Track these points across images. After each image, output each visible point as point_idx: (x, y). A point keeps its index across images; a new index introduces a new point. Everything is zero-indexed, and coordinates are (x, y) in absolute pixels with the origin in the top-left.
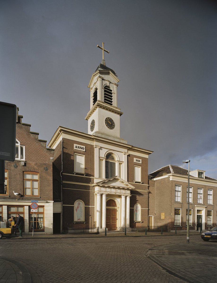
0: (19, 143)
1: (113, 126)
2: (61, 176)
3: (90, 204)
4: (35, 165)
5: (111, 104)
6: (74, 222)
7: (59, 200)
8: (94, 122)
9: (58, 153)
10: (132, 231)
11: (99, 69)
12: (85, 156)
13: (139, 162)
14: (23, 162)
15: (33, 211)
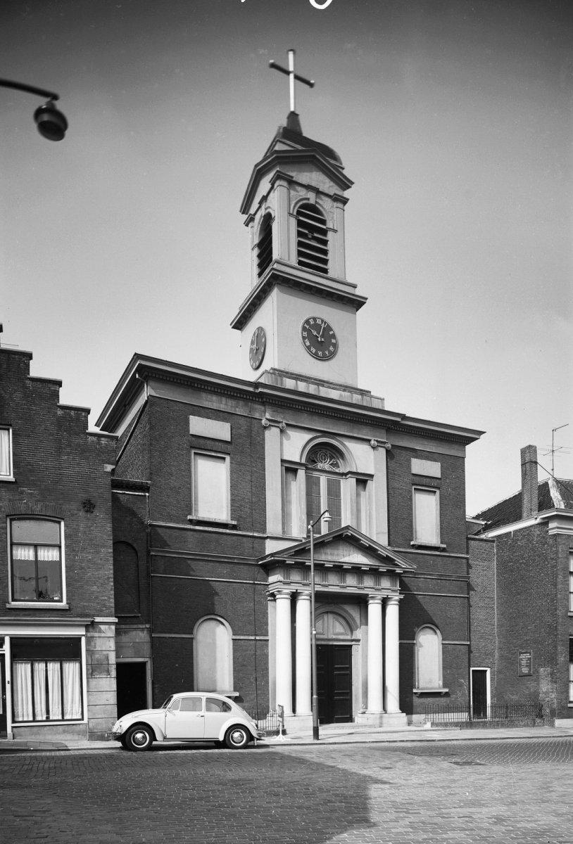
5: (325, 271)
7: (140, 615)
8: (265, 336)
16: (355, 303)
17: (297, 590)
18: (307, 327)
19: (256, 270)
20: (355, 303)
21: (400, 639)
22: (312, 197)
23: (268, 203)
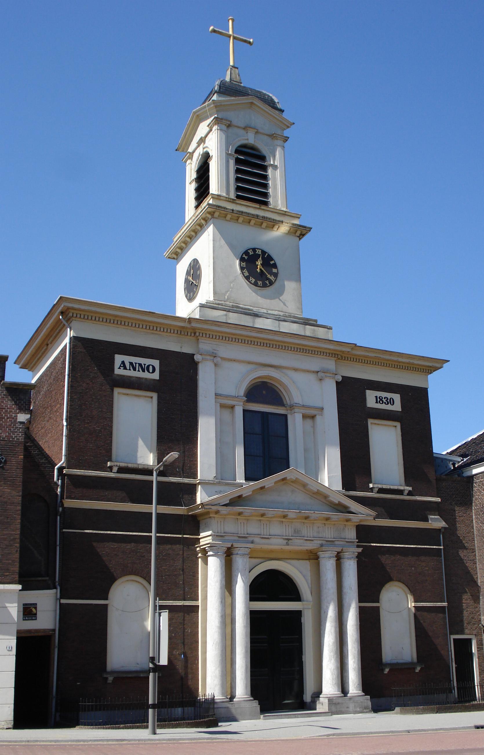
5: (266, 203)
6: (105, 676)
7: (47, 578)
8: (199, 268)
11: (215, 97)
18: (246, 257)
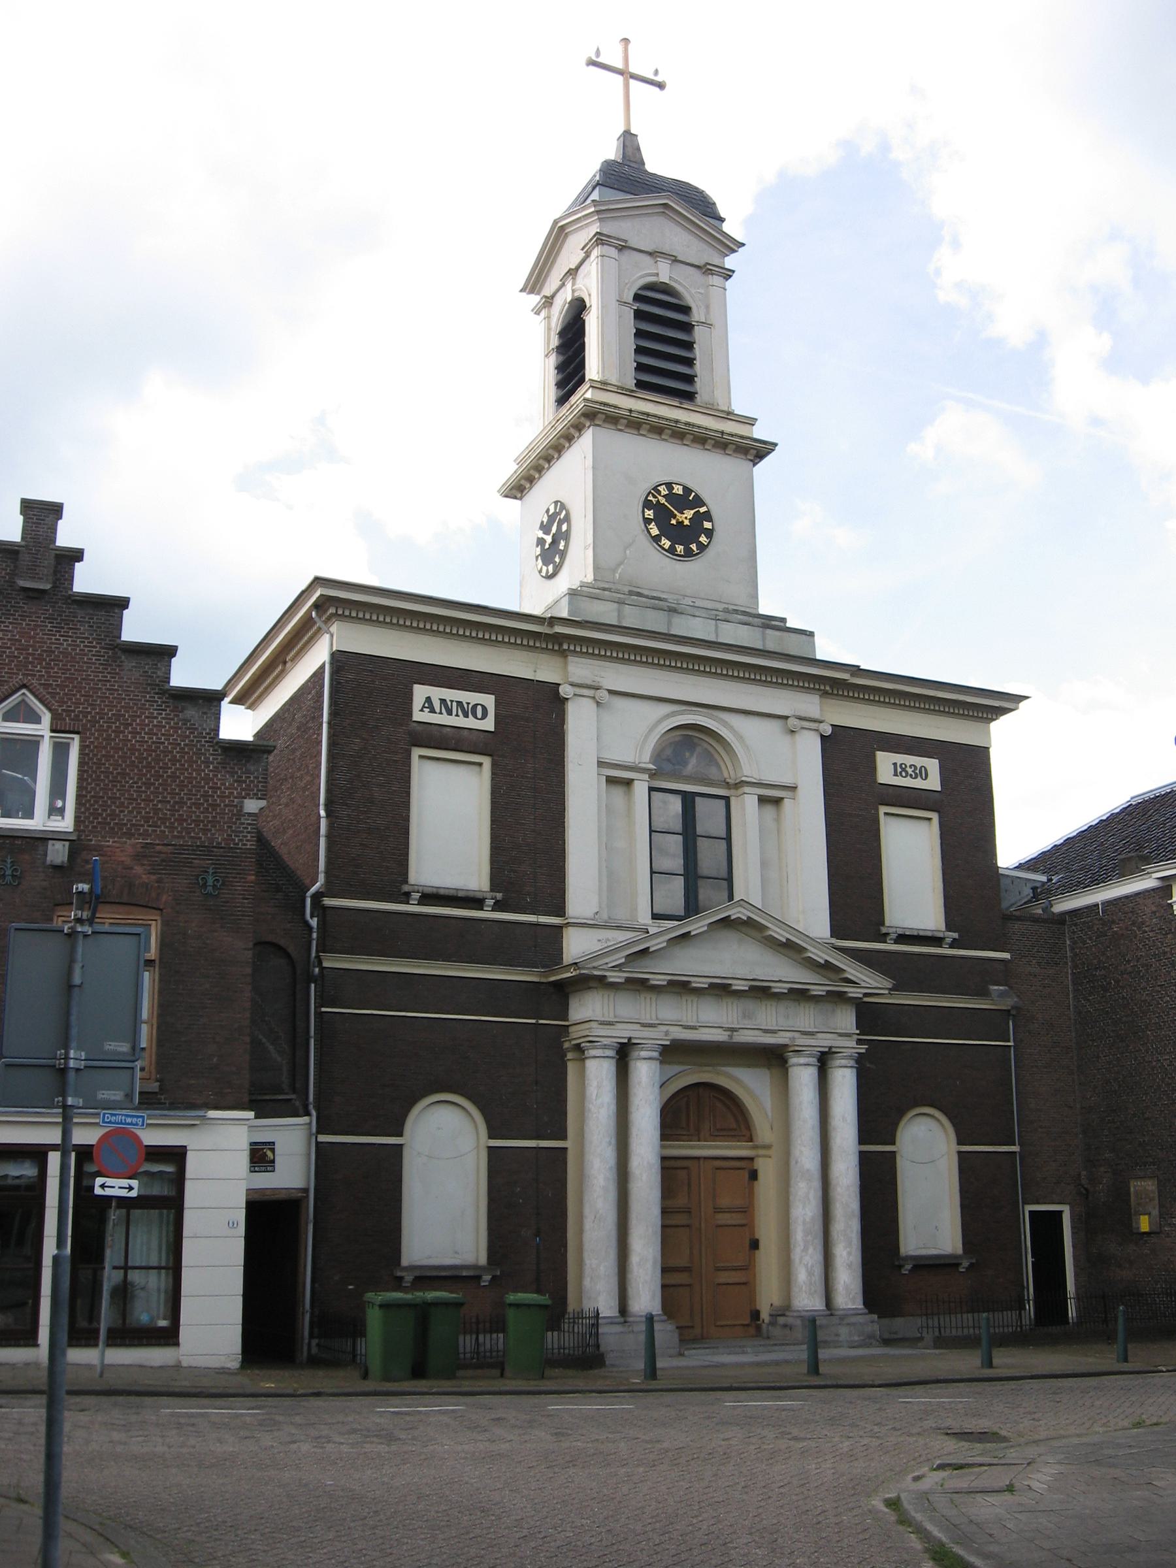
0: (47, 717)
1: (703, 539)
2: (314, 922)
3: (307, 881)
4: (138, 857)
5: (690, 396)
6: (399, 1274)
7: (293, 1096)
9: (294, 751)
10: (887, 1342)
12: (494, 765)
13: (918, 783)
14: (59, 845)
15: (108, 1192)
16: (758, 451)
17: (630, 1039)
19: (552, 393)
20: (758, 451)
21: (862, 1140)
22: (664, 273)
23: (581, 282)
